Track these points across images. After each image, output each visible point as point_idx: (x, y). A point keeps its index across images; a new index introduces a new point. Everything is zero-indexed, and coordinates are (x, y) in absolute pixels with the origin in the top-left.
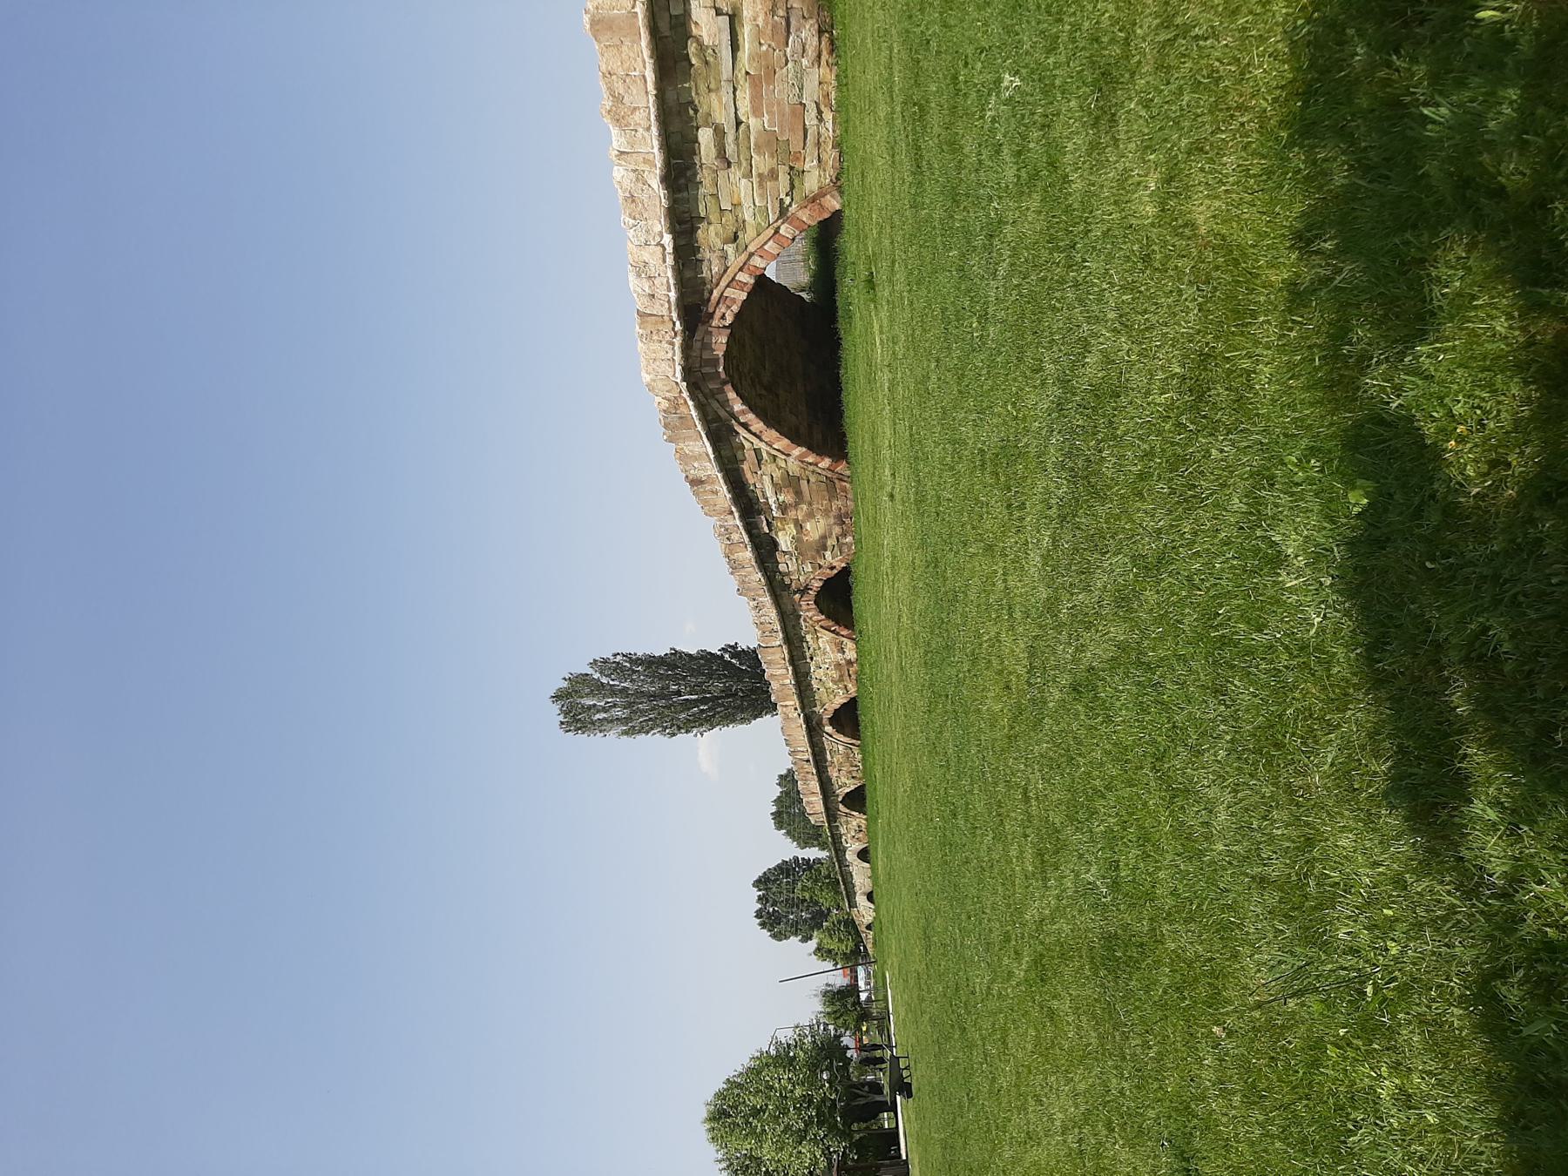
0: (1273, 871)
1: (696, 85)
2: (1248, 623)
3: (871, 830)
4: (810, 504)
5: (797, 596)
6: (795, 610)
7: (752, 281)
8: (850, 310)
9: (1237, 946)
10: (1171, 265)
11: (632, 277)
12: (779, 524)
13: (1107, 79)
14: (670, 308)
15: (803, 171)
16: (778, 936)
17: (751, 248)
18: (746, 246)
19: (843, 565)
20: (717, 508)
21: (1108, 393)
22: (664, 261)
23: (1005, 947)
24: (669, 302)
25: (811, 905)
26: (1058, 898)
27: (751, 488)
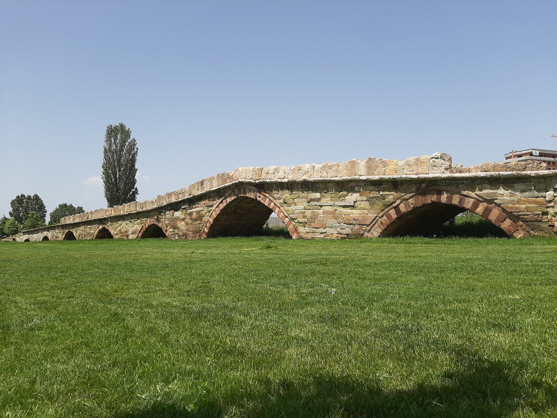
0: (38, 386)
1: (333, 193)
2: (142, 373)
3: (56, 242)
4: (191, 224)
5: (156, 217)
6: (150, 216)
7: (271, 208)
8: (259, 241)
9: (4, 374)
10: (275, 342)
11: (274, 167)
12: (184, 212)
13: (334, 320)
14: (263, 179)
15: (305, 227)
16: (13, 203)
17: (281, 208)
18: (282, 206)
19: (167, 235)
20: (192, 190)
21: (230, 322)
22: (279, 178)
23: (4, 289)
24: (265, 179)
25: (26, 217)
26: (26, 309)
27: (199, 203)
